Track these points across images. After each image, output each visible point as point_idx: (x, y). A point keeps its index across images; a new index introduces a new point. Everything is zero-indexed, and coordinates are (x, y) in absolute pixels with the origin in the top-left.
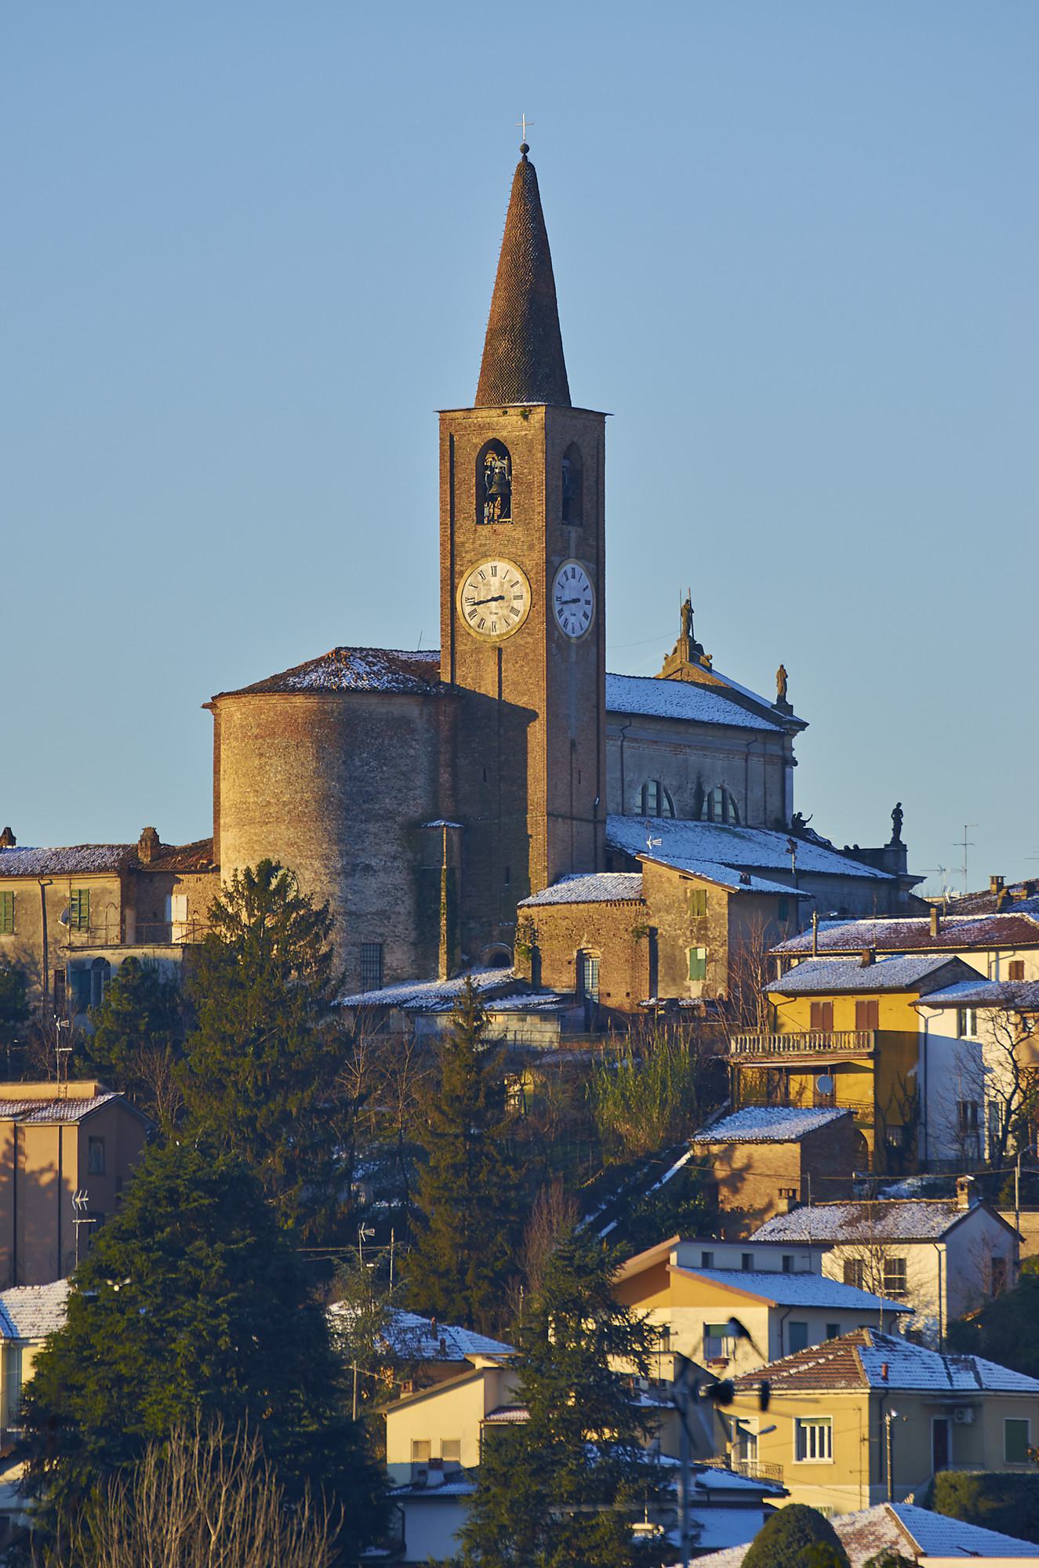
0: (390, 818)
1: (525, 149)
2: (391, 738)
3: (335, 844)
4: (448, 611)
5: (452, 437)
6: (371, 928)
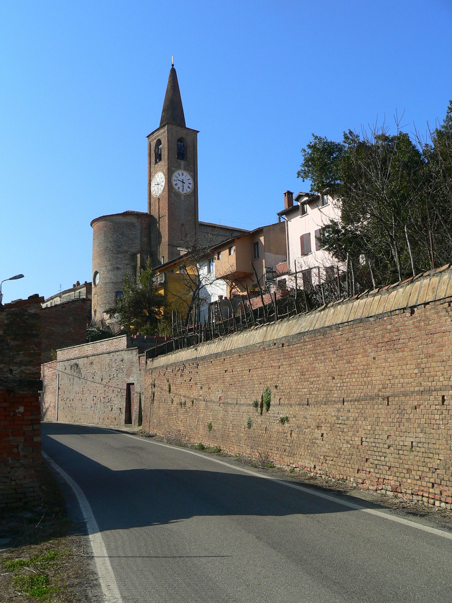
0: (126, 253)
1: (173, 65)
2: (126, 229)
3: (109, 262)
4: (149, 192)
5: (150, 143)
6: (119, 286)
